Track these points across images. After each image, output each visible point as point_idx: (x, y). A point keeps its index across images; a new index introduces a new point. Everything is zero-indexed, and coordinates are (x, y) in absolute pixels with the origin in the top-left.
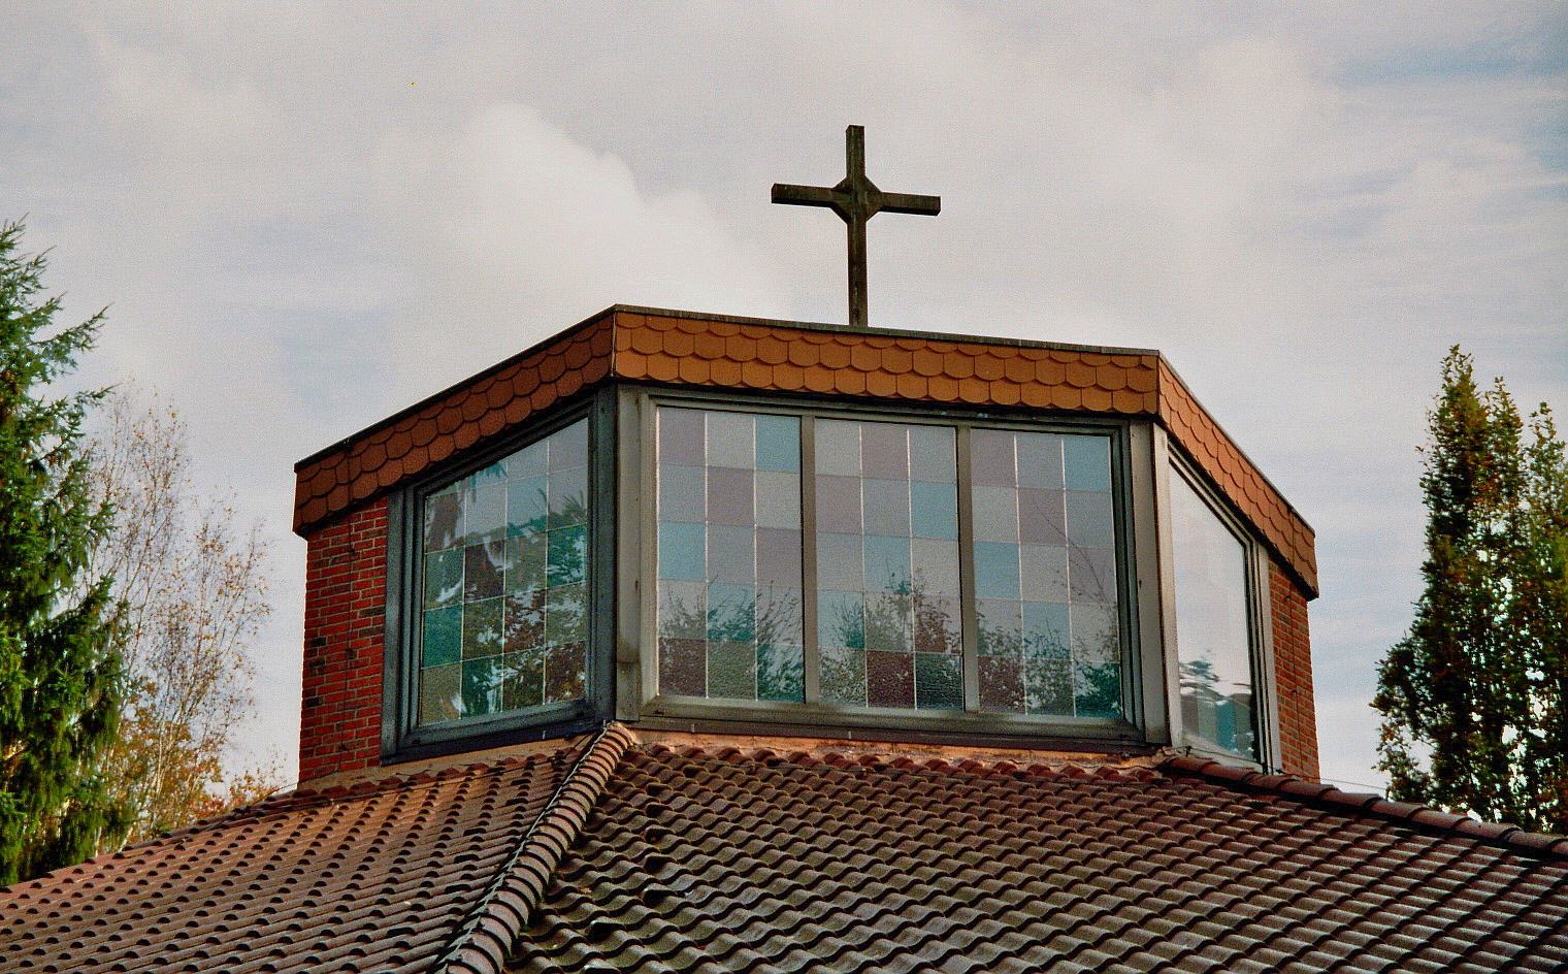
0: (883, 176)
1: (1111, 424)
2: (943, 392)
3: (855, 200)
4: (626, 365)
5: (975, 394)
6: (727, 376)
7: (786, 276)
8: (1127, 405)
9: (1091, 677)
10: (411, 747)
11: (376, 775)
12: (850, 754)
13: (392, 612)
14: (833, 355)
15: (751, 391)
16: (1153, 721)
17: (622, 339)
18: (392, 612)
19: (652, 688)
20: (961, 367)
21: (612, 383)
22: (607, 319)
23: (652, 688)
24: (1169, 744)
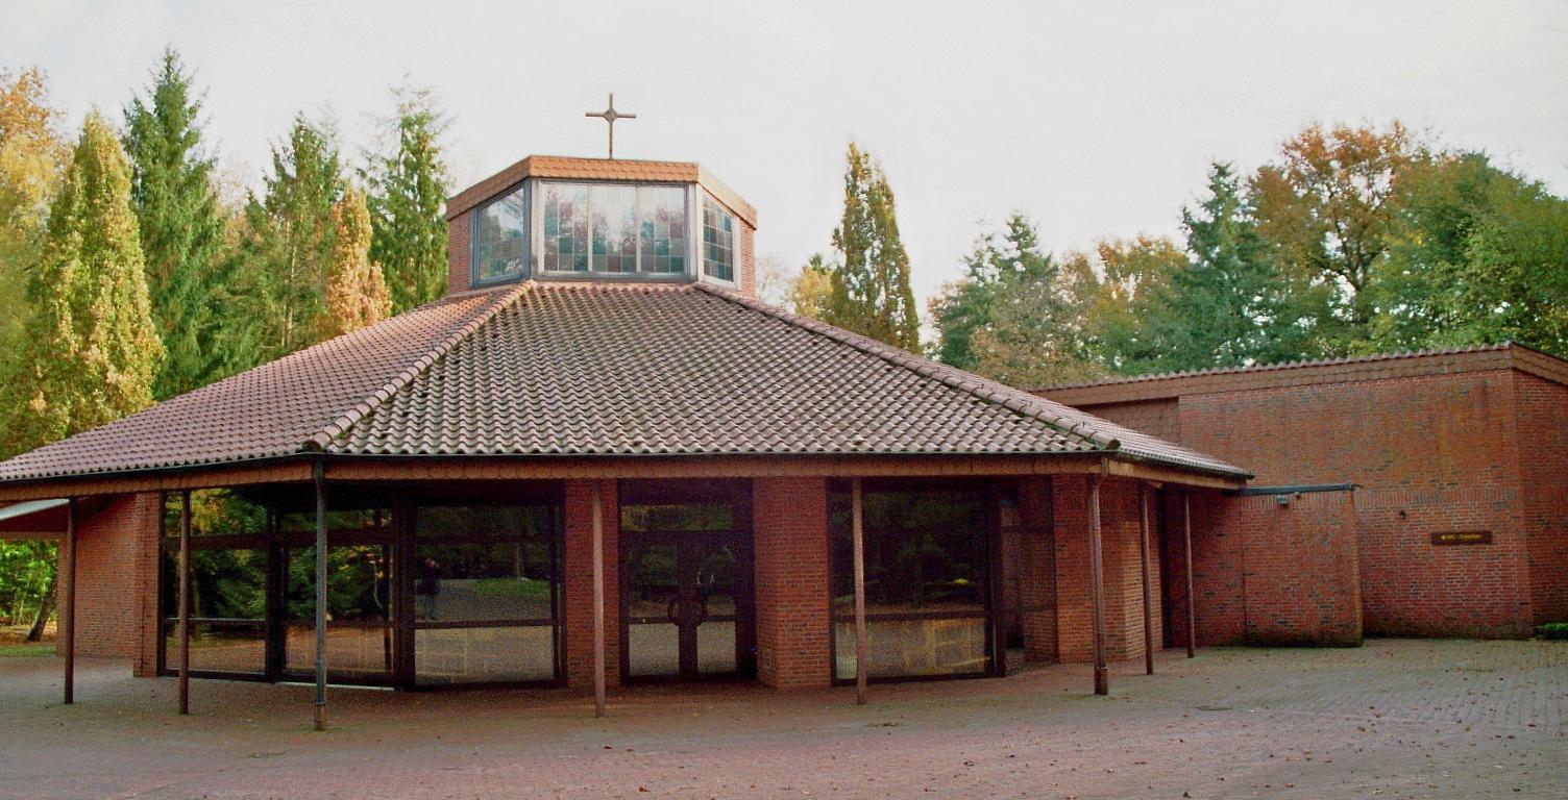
0: (618, 109)
1: (684, 184)
2: (631, 177)
3: (610, 116)
4: (534, 172)
5: (641, 177)
6: (565, 174)
7: (590, 143)
8: (688, 179)
9: (108, 246)
10: (477, 286)
11: (468, 293)
12: (671, 289)
13: (472, 246)
14: (606, 166)
15: (658, 181)
16: (693, 273)
17: (532, 164)
18: (472, 246)
19: (541, 268)
20: (637, 168)
21: (529, 177)
22: (529, 159)
23: (541, 268)
24: (697, 280)
